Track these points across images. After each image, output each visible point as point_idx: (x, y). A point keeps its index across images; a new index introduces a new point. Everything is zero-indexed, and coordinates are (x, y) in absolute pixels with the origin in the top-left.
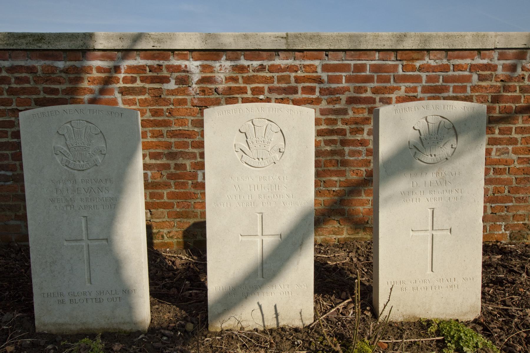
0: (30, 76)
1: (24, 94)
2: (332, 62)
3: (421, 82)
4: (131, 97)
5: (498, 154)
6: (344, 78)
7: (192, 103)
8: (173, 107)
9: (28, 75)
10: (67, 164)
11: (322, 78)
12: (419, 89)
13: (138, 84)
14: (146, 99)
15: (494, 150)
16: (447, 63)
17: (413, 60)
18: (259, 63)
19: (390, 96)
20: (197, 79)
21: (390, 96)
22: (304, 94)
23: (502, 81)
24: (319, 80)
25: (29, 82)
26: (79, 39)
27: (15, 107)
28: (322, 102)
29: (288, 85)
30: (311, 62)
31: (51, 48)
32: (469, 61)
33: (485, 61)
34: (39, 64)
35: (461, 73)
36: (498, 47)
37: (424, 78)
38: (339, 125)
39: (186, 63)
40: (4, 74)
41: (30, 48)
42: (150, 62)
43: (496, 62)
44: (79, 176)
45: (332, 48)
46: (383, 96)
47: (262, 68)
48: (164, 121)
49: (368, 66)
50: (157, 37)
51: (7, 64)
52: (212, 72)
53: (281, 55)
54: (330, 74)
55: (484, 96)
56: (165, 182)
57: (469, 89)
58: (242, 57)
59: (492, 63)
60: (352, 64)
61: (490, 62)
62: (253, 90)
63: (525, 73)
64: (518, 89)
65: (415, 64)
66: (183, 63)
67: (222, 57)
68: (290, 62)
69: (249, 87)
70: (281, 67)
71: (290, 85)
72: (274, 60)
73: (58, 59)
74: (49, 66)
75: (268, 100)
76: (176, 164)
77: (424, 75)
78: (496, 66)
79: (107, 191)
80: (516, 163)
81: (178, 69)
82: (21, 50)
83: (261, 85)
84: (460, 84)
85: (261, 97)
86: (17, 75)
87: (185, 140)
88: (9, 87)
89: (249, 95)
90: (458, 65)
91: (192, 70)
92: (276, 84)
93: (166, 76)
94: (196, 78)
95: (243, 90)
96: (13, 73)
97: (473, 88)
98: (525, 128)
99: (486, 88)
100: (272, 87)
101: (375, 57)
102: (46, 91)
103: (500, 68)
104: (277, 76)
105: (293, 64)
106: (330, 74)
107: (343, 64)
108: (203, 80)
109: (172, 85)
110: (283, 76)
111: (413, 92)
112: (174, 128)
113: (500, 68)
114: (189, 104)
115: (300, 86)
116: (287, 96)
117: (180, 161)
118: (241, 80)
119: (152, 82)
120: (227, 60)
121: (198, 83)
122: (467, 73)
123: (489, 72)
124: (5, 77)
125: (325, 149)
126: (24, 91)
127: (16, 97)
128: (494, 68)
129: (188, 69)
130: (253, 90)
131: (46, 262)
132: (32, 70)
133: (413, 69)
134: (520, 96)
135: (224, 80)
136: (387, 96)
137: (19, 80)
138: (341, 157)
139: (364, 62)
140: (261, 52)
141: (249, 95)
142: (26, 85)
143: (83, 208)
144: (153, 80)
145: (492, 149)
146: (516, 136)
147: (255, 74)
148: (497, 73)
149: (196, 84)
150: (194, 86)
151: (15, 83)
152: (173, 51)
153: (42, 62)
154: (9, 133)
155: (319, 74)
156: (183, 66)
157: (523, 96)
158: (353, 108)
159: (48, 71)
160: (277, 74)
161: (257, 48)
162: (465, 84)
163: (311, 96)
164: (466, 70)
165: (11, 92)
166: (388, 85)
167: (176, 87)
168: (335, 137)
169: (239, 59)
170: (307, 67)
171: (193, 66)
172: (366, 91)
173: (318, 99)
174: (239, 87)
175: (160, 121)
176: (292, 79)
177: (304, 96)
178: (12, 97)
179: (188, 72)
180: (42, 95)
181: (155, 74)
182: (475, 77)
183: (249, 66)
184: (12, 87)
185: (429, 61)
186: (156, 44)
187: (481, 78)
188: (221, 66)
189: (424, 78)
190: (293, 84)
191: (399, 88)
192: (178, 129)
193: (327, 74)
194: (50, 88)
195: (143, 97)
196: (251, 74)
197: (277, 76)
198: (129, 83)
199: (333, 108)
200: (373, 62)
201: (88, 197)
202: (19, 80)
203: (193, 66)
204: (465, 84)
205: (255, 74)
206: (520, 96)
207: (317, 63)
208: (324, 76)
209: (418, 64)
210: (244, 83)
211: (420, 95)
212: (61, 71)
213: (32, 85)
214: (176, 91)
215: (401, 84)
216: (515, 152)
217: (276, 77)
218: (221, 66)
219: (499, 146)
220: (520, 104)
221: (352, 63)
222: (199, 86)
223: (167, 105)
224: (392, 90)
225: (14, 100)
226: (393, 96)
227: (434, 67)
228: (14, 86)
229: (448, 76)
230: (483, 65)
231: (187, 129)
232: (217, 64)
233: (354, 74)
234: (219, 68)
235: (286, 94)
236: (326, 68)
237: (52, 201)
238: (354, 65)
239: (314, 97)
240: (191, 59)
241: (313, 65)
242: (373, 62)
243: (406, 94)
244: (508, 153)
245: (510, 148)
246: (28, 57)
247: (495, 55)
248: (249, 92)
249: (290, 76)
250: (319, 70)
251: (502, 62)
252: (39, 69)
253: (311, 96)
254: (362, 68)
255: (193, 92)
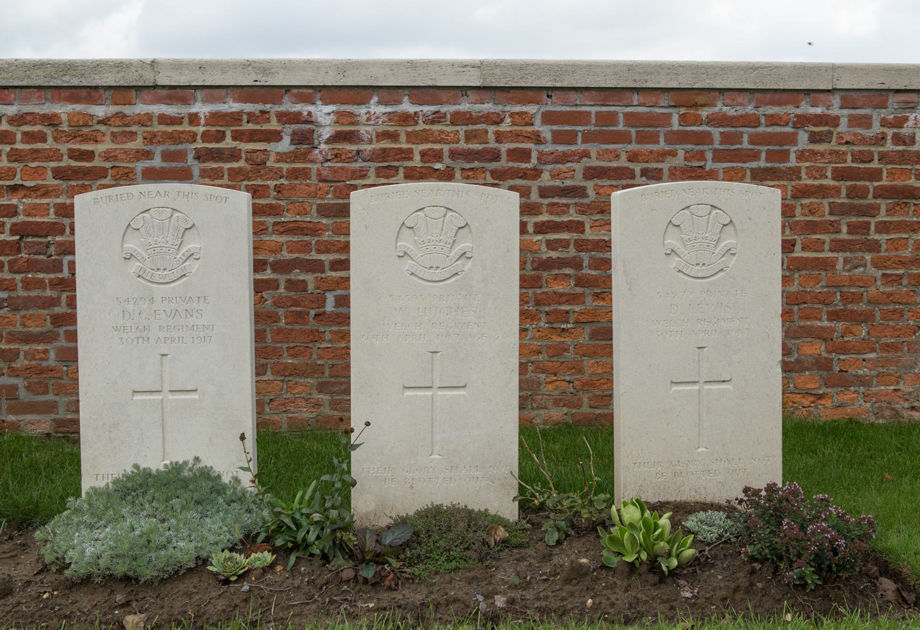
0: (48, 131)
1: (34, 160)
2: (558, 109)
3: (711, 142)
4: (215, 165)
5: (847, 267)
6: (580, 134)
7: (319, 175)
8: (286, 183)
9: (45, 129)
10: (141, 273)
11: (543, 135)
12: (709, 155)
13: (228, 143)
14: (240, 168)
15: (841, 260)
16: (753, 111)
17: (696, 106)
18: (434, 108)
19: (660, 165)
20: (328, 135)
21: (660, 165)
22: (511, 161)
23: (847, 143)
24: (537, 139)
25: (44, 140)
26: (133, 69)
27: (20, 182)
28: (543, 175)
29: (484, 146)
30: (525, 109)
31: (85, 84)
32: (791, 110)
33: (819, 110)
34: (63, 110)
35: (778, 129)
36: (838, 87)
37: (717, 138)
38: (571, 215)
39: (311, 108)
40: (5, 126)
41: (51, 84)
42: (248, 107)
43: (835, 111)
44: (160, 291)
45: (558, 85)
46: (646, 165)
47: (437, 118)
48: (271, 206)
49: (621, 115)
50: (262, 66)
51: (11, 110)
52: (353, 124)
53: (471, 97)
54: (555, 128)
55: (819, 168)
56: (268, 312)
57: (793, 157)
58: (406, 99)
59: (830, 112)
60: (593, 113)
61: (826, 112)
62: (423, 154)
63: (885, 130)
64: (876, 157)
65: (699, 113)
66: (304, 109)
67: (371, 98)
68: (488, 107)
69: (418, 148)
70: (471, 115)
71: (487, 145)
72: (460, 104)
73: (95, 102)
74: (80, 113)
75: (447, 175)
76: (289, 281)
77: (716, 132)
78: (837, 118)
79: (199, 316)
80: (879, 283)
81: (295, 118)
82: (35, 87)
83: (437, 146)
84: (777, 148)
85: (438, 166)
86: (27, 128)
87: (306, 238)
88: (12, 149)
89: (417, 161)
90: (772, 116)
91: (320, 119)
92: (463, 145)
93: (276, 131)
94: (326, 133)
95: (407, 155)
96: (20, 126)
97: (801, 156)
98: (891, 223)
99: (822, 155)
100: (456, 149)
101: (632, 101)
102: (73, 154)
103: (844, 121)
104: (466, 131)
105: (492, 111)
106: (555, 128)
107: (577, 112)
108: (338, 137)
109: (285, 145)
110: (475, 130)
111: (699, 160)
112: (288, 217)
113: (844, 121)
114: (314, 177)
115: (504, 147)
116: (482, 164)
117: (297, 275)
118: (403, 138)
119: (250, 140)
120: (379, 103)
121: (328, 142)
122: (788, 129)
123: (826, 128)
124: (6, 131)
125: (548, 255)
126: (35, 154)
127: (21, 165)
128: (834, 121)
129: (314, 119)
130: (423, 154)
131: (104, 424)
132: (51, 120)
133: (698, 121)
134: (881, 170)
135: (374, 137)
136: (654, 165)
137: (29, 137)
138: (576, 269)
139: (613, 109)
140: (438, 92)
141: (417, 161)
142: (39, 146)
143: (163, 341)
144: (252, 136)
145: (837, 258)
146: (877, 237)
147: (427, 127)
148: (839, 129)
149: (326, 143)
150: (323, 146)
151: (22, 142)
152: (288, 89)
153: (70, 108)
154: (8, 226)
155: (536, 128)
156: (305, 113)
157: (884, 170)
158: (596, 185)
159: (78, 121)
160: (465, 128)
161: (430, 83)
162: (787, 147)
163: (523, 165)
164: (787, 124)
165: (15, 156)
166: (655, 147)
167: (293, 148)
168: (564, 236)
169: (400, 102)
170: (517, 117)
171: (323, 113)
172: (618, 156)
173: (535, 169)
174: (400, 149)
175: (263, 205)
176: (491, 137)
177: (511, 164)
178: (15, 165)
179: (311, 122)
180: (66, 162)
181: (258, 127)
182: (803, 137)
183: (415, 113)
184: (17, 149)
185: (720, 107)
186: (259, 77)
187: (814, 138)
188: (368, 112)
189: (717, 138)
190: (493, 145)
191: (674, 154)
192: (294, 219)
193: (550, 127)
194: (79, 150)
195: (235, 165)
196: (421, 126)
197: (466, 131)
198: (212, 142)
199: (561, 185)
200: (629, 109)
201: (170, 324)
202: (29, 137)
203: (323, 113)
204: (787, 147)
205: (427, 127)
206: (881, 170)
207: (531, 109)
208: (546, 131)
209: (704, 113)
210: (408, 142)
211: (710, 165)
212: (99, 122)
213: (50, 144)
214: (292, 155)
215: (677, 147)
216: (876, 265)
217: (462, 133)
218: (368, 112)
219: (848, 254)
220: (880, 183)
221: (594, 110)
222: (331, 146)
223: (276, 179)
224: (662, 156)
225: (18, 170)
226: (664, 166)
227: (733, 117)
228: (19, 146)
229: (758, 134)
230: (816, 116)
231: (308, 219)
232: (362, 110)
233: (598, 128)
234: (365, 117)
235: (481, 161)
236: (549, 118)
237: (116, 329)
238: (597, 113)
239: (528, 166)
240: (319, 102)
241: (526, 113)
242: (629, 109)
243: (686, 163)
244: (865, 266)
245: (868, 257)
246: (46, 99)
247: (836, 100)
248: (417, 157)
249: (487, 132)
250: (538, 120)
251: (846, 112)
252: (64, 117)
253: (523, 165)
254: (610, 118)
255: (320, 158)
